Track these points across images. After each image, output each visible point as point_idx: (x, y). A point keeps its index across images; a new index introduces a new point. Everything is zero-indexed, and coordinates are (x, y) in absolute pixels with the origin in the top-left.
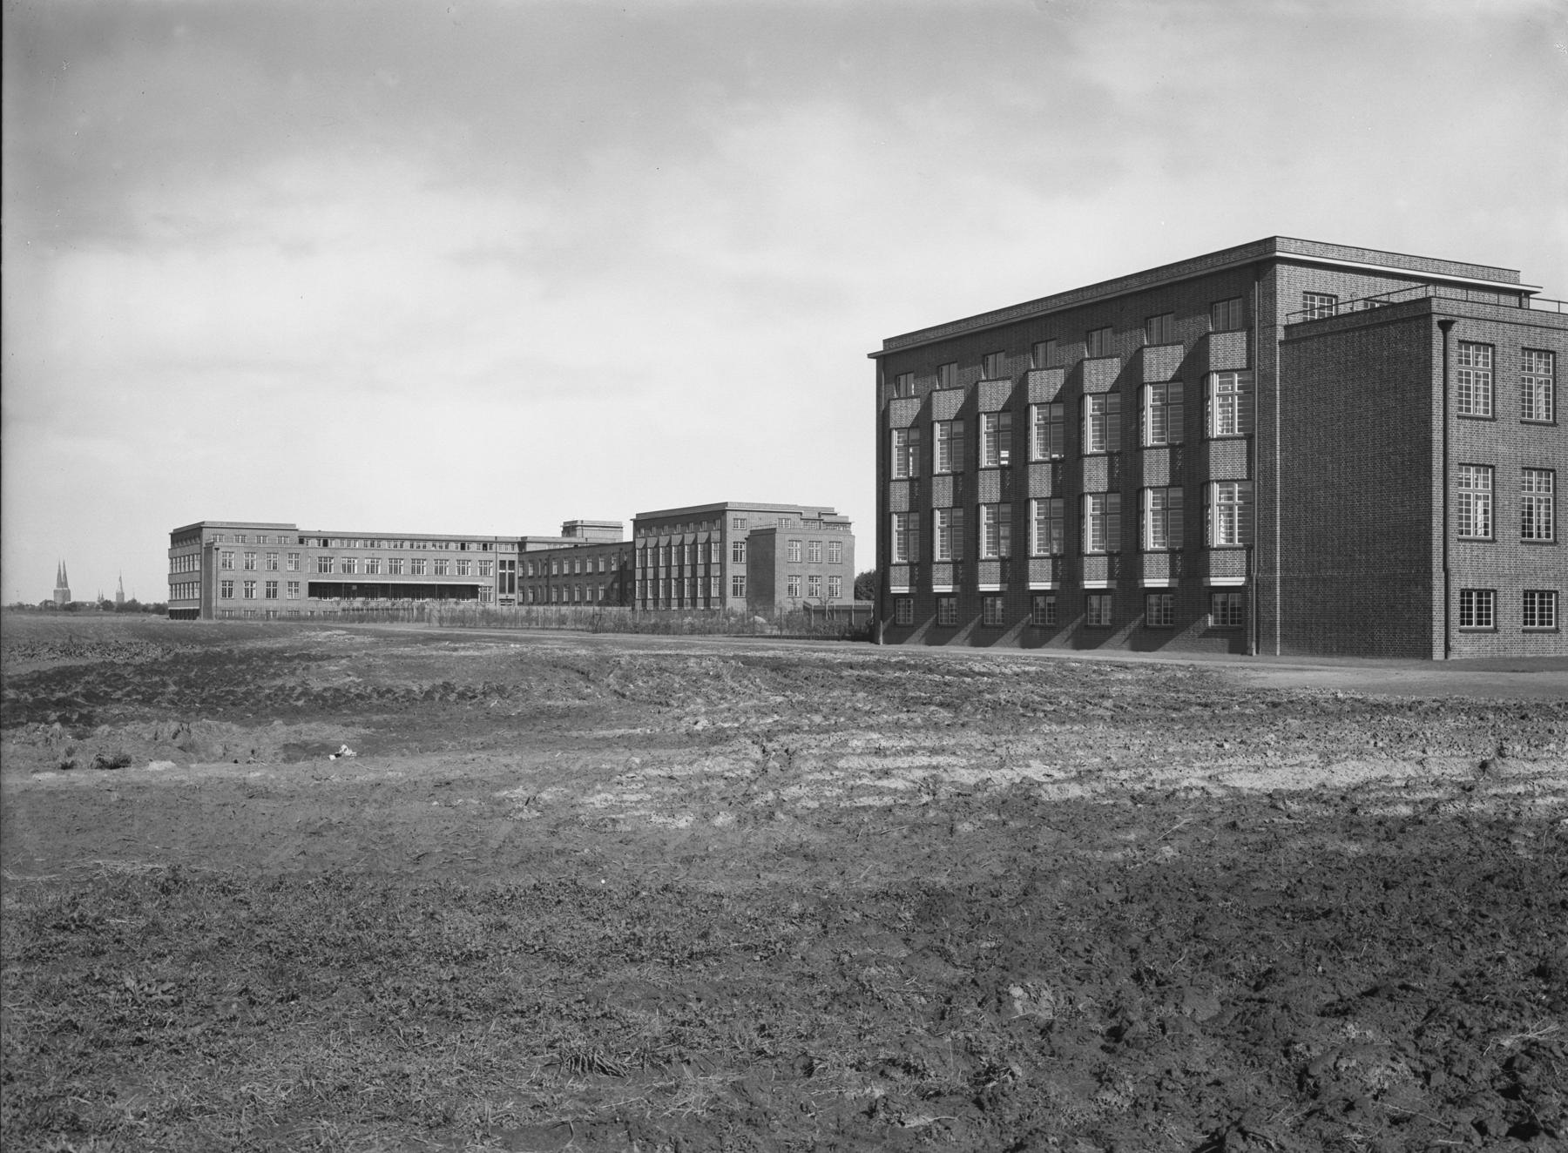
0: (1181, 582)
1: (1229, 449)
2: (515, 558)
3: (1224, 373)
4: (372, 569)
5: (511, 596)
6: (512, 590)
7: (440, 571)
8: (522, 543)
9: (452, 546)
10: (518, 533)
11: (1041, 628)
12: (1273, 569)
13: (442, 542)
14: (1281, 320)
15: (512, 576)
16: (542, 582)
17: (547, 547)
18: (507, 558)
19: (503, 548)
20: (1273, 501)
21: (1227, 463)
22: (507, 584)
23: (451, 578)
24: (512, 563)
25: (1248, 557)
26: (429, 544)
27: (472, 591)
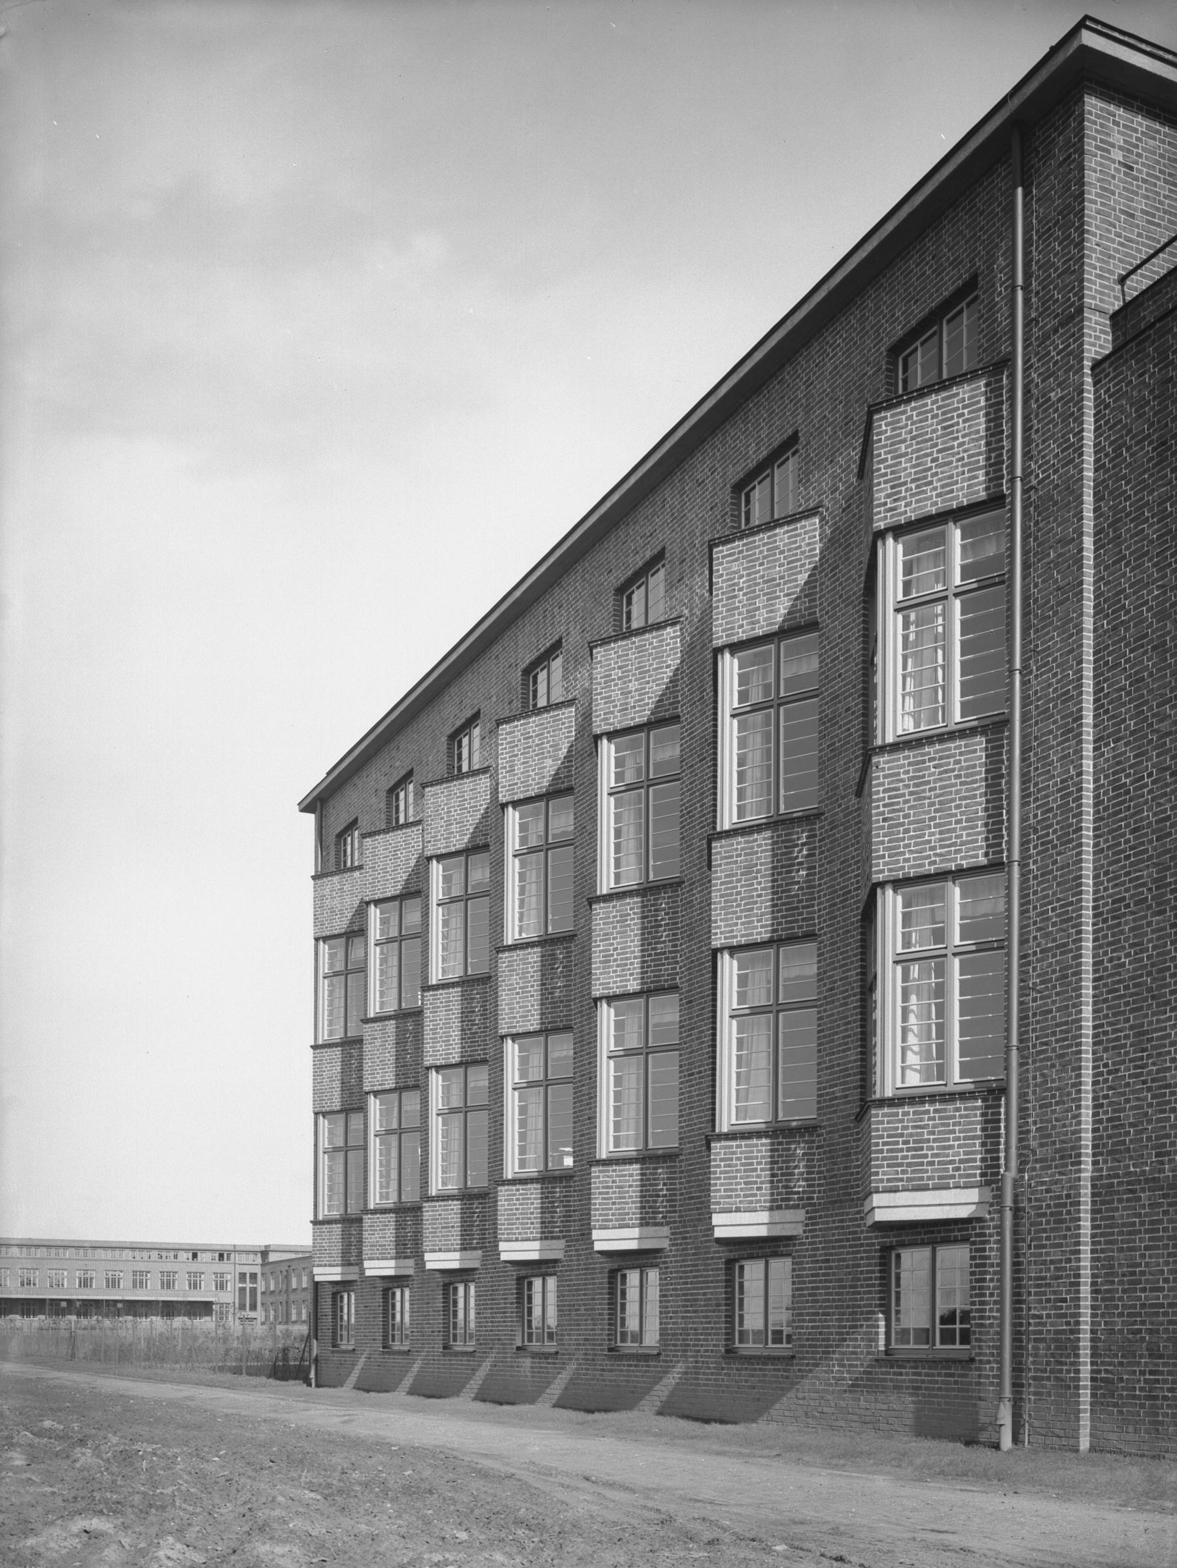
0: (811, 1220)
1: (931, 772)
2: (257, 1270)
3: (922, 528)
4: (85, 1283)
5: (252, 1314)
6: (253, 1307)
7: (168, 1285)
8: (265, 1253)
9: (183, 1256)
10: (260, 1241)
11: (535, 1355)
12: (1069, 1155)
13: (176, 1250)
14: (1102, 294)
15: (253, 1291)
16: (283, 1298)
17: (293, 1256)
18: (248, 1270)
19: (244, 1258)
20: (1069, 976)
21: (927, 813)
22: (247, 1300)
23: (181, 1293)
24: (254, 1276)
25: (991, 1123)
26: (154, 1254)
27: (204, 1308)
